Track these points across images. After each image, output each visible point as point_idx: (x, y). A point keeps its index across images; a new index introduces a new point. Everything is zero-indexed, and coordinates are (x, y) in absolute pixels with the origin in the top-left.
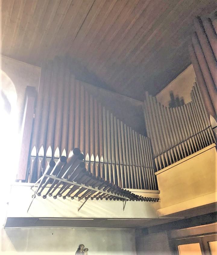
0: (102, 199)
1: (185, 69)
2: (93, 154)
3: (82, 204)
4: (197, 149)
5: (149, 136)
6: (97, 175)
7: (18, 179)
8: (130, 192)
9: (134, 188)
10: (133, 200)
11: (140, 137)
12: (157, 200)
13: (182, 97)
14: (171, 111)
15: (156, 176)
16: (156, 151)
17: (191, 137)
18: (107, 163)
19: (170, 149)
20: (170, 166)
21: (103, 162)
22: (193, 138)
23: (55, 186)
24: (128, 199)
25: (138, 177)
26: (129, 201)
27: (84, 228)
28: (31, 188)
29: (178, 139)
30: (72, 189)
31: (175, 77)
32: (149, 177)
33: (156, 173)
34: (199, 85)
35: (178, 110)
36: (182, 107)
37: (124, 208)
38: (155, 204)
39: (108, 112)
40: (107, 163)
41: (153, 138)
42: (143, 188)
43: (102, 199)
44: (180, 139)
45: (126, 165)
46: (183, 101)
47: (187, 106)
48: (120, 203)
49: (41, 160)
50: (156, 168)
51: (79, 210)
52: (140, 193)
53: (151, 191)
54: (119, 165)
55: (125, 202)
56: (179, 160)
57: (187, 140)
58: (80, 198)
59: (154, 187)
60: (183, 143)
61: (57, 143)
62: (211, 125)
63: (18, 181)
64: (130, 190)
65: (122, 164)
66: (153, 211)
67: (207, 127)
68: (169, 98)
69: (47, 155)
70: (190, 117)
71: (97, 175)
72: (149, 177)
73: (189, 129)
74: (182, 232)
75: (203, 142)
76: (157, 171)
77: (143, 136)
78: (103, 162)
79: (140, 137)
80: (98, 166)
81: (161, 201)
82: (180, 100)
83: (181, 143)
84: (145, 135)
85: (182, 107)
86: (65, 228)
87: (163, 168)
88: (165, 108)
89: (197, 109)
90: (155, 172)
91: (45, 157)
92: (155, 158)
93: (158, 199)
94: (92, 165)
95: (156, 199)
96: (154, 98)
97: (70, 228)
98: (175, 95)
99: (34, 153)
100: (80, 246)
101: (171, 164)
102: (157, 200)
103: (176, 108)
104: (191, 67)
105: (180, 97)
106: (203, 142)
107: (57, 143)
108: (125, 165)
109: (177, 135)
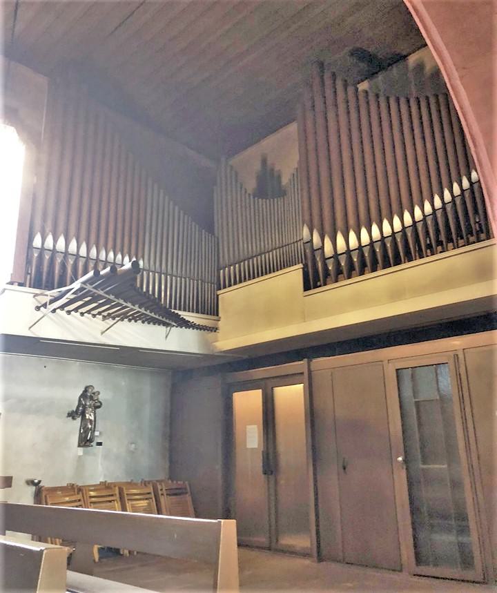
0: (136, 321)
2: (86, 241)
3: (109, 326)
5: (216, 235)
6: (144, 290)
8: (180, 315)
9: (185, 310)
10: (181, 327)
12: (214, 329)
15: (218, 296)
18: (149, 271)
19: (245, 260)
20: (241, 285)
23: (86, 299)
26: (175, 328)
27: (93, 364)
30: (86, 302)
32: (208, 296)
33: (219, 292)
36: (272, 200)
37: (166, 337)
38: (211, 335)
39: (177, 208)
40: (149, 271)
42: (197, 312)
43: (136, 321)
48: (162, 329)
50: (220, 284)
51: (102, 333)
52: (192, 318)
53: (209, 317)
55: (169, 328)
58: (105, 318)
59: (214, 311)
64: (180, 313)
66: (206, 344)
68: (257, 166)
69: (69, 250)
72: (208, 296)
74: (242, 375)
76: (220, 289)
78: (112, 261)
79: (203, 233)
80: (73, 264)
81: (220, 331)
82: (276, 174)
86: (64, 360)
87: (230, 286)
88: (247, 195)
91: (88, 258)
93: (217, 329)
94: (47, 257)
95: (213, 328)
98: (269, 162)
99: (37, 242)
102: (214, 329)
104: (293, 128)
105: (277, 169)
108: (152, 271)
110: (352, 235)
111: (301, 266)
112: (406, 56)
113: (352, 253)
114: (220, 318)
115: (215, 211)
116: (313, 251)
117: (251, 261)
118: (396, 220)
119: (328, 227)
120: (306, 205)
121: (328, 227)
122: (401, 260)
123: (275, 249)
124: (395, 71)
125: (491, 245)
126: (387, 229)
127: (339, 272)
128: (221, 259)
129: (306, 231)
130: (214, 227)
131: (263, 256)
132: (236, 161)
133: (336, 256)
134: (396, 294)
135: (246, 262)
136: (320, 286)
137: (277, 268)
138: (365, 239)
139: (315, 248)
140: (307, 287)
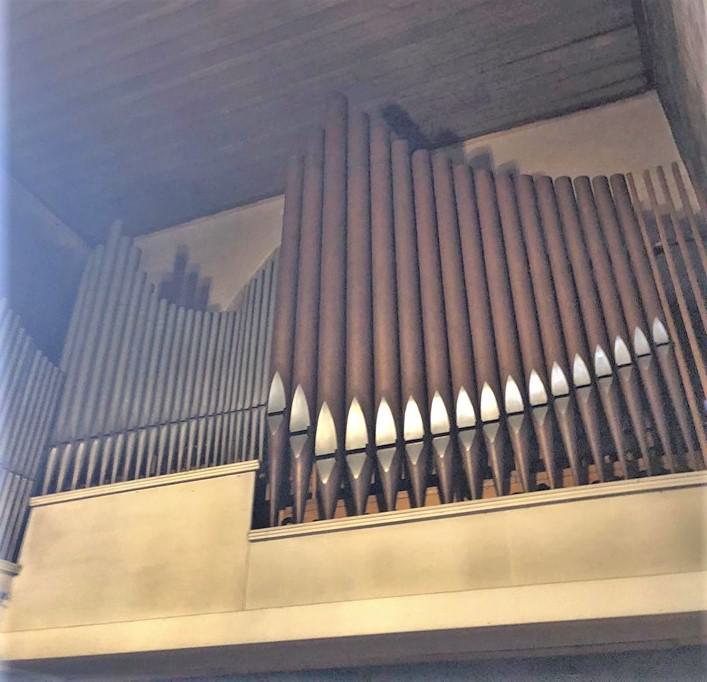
1: (193, 218)
4: (192, 459)
5: (63, 368)
11: (37, 358)
13: (209, 280)
14: (172, 315)
15: (29, 509)
16: (71, 420)
17: (198, 418)
19: (118, 433)
22: (203, 421)
29: (157, 409)
31: (214, 210)
33: (35, 501)
41: (77, 374)
44: (140, 415)
46: (206, 290)
47: (223, 321)
56: (131, 477)
57: (153, 426)
67: (255, 403)
68: (168, 266)
70: (219, 353)
73: (233, 383)
75: (195, 450)
76: (38, 493)
79: (37, 358)
84: (54, 353)
85: (199, 314)
89: (247, 336)
90: (32, 496)
92: (54, 446)
96: (125, 241)
101: (85, 483)
104: (278, 203)
105: (203, 274)
106: (195, 450)
109: (159, 394)
110: (412, 410)
111: (254, 464)
112: (464, 139)
113: (379, 452)
114: (20, 567)
115: (72, 330)
116: (287, 434)
117: (132, 436)
118: (488, 397)
119: (328, 384)
120: (283, 336)
121: (328, 384)
122: (268, 519)
123: (198, 418)
125: (700, 485)
127: (375, 488)
128: (61, 420)
129: (277, 388)
130: (61, 347)
131: (164, 430)
132: (142, 242)
133: (372, 448)
134: (483, 571)
135: (120, 438)
136: (544, 487)
137: (226, 457)
138: (413, 426)
139: (293, 427)
140: (261, 518)
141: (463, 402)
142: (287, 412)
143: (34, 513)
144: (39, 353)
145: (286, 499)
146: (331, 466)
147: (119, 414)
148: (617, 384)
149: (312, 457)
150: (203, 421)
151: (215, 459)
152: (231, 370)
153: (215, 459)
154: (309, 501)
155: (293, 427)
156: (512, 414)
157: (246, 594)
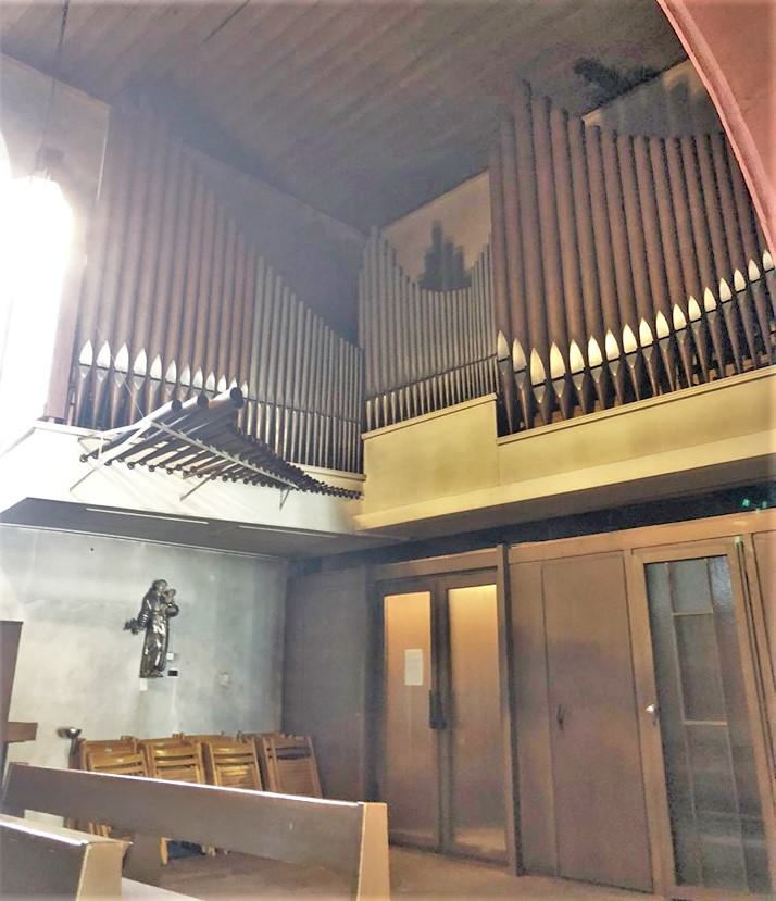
7: (47, 415)
9: (310, 464)
13: (461, 247)
15: (362, 441)
18: (256, 402)
20: (399, 425)
21: (201, 387)
22: (457, 371)
23: (160, 445)
24: (294, 485)
25: (321, 441)
27: (168, 545)
28: (79, 439)
32: (347, 444)
33: (364, 436)
34: (494, 273)
35: (436, 366)
37: (281, 505)
38: (351, 503)
40: (256, 402)
42: (330, 467)
45: (298, 411)
49: (102, 375)
51: (183, 498)
54: (283, 408)
59: (356, 465)
60: (434, 379)
61: (232, 373)
62: (496, 354)
63: (45, 419)
64: (303, 467)
65: (272, 402)
66: (343, 517)
67: (490, 354)
71: (249, 432)
72: (347, 444)
74: (399, 569)
76: (365, 431)
77: (347, 343)
78: (201, 387)
82: (455, 253)
83: (430, 378)
84: (353, 338)
86: (121, 539)
87: (382, 425)
88: (410, 285)
91: (163, 381)
93: (360, 494)
95: (355, 492)
97: (133, 541)
100: (154, 587)
102: (356, 494)
103: (442, 294)
104: (483, 181)
105: (457, 244)
107: (232, 373)
111: (493, 396)
115: (361, 317)
118: (644, 328)
119: (536, 336)
121: (536, 336)
123: (454, 369)
124: (643, 94)
126: (663, 327)
129: (501, 343)
132: (395, 231)
134: (644, 444)
136: (524, 429)
139: (516, 368)
140: (503, 430)
141: (556, 356)
142: (510, 358)
143: (366, 443)
144: (342, 340)
145: (518, 416)
146: (581, 380)
147: (404, 375)
148: (736, 306)
149: (531, 387)
150: (457, 371)
151: (447, 401)
152: (439, 346)
153: (447, 401)
154: (555, 414)
155: (516, 368)
156: (519, 372)
157: (499, 476)
